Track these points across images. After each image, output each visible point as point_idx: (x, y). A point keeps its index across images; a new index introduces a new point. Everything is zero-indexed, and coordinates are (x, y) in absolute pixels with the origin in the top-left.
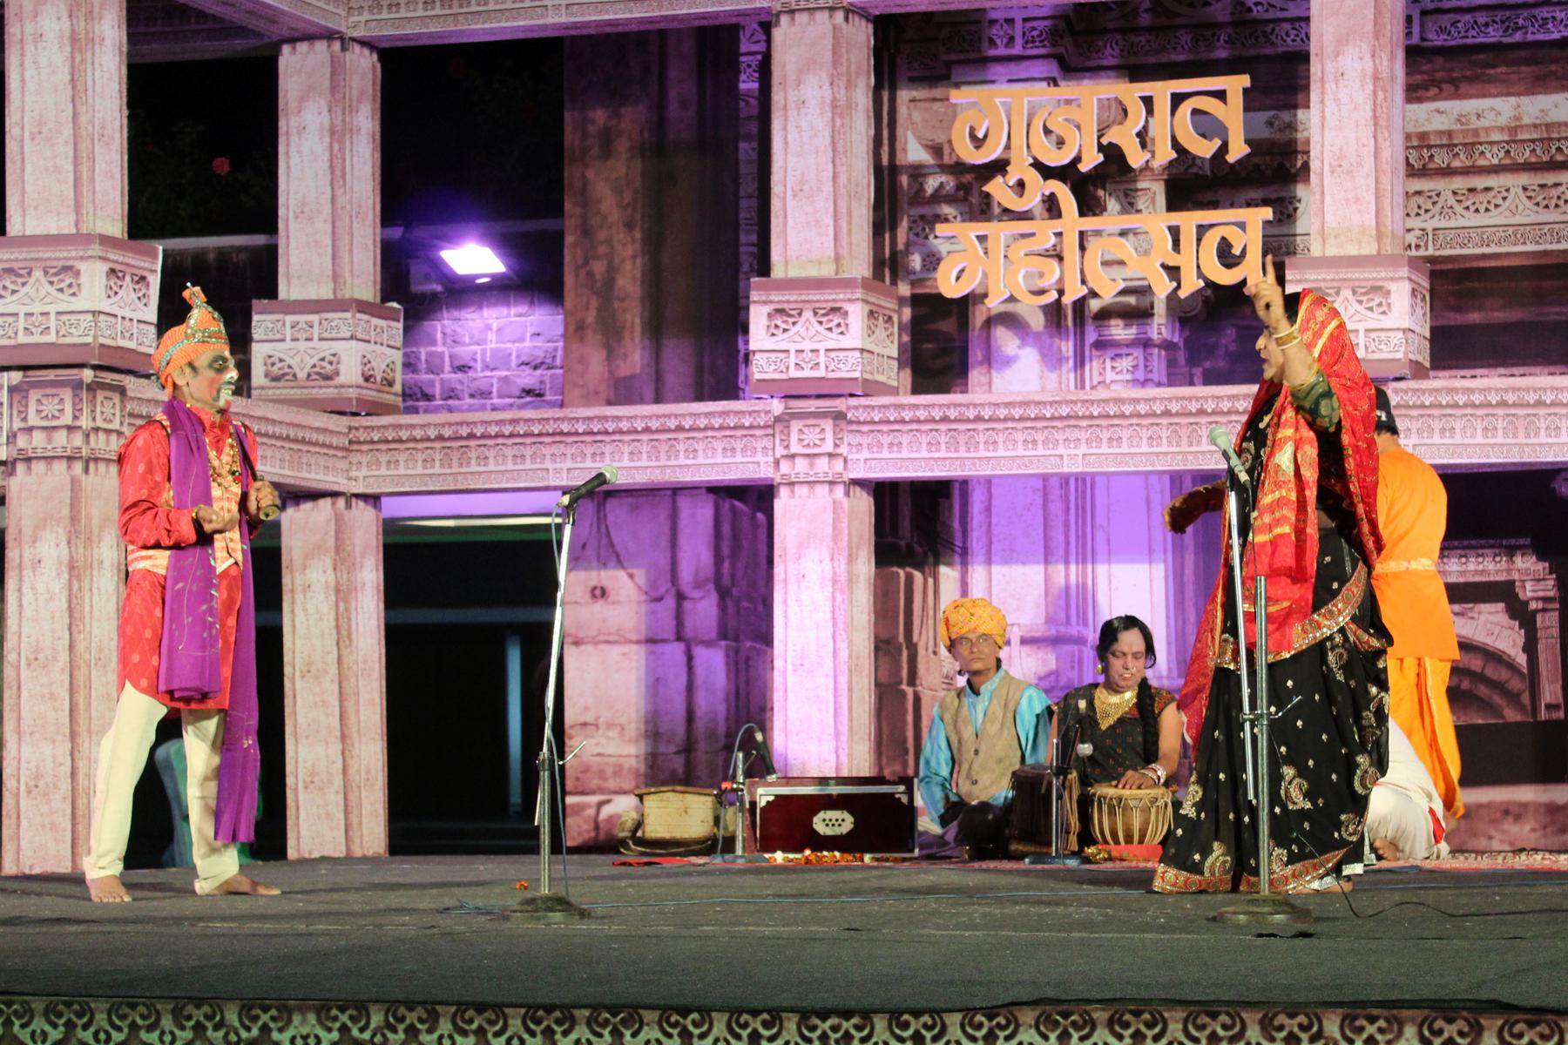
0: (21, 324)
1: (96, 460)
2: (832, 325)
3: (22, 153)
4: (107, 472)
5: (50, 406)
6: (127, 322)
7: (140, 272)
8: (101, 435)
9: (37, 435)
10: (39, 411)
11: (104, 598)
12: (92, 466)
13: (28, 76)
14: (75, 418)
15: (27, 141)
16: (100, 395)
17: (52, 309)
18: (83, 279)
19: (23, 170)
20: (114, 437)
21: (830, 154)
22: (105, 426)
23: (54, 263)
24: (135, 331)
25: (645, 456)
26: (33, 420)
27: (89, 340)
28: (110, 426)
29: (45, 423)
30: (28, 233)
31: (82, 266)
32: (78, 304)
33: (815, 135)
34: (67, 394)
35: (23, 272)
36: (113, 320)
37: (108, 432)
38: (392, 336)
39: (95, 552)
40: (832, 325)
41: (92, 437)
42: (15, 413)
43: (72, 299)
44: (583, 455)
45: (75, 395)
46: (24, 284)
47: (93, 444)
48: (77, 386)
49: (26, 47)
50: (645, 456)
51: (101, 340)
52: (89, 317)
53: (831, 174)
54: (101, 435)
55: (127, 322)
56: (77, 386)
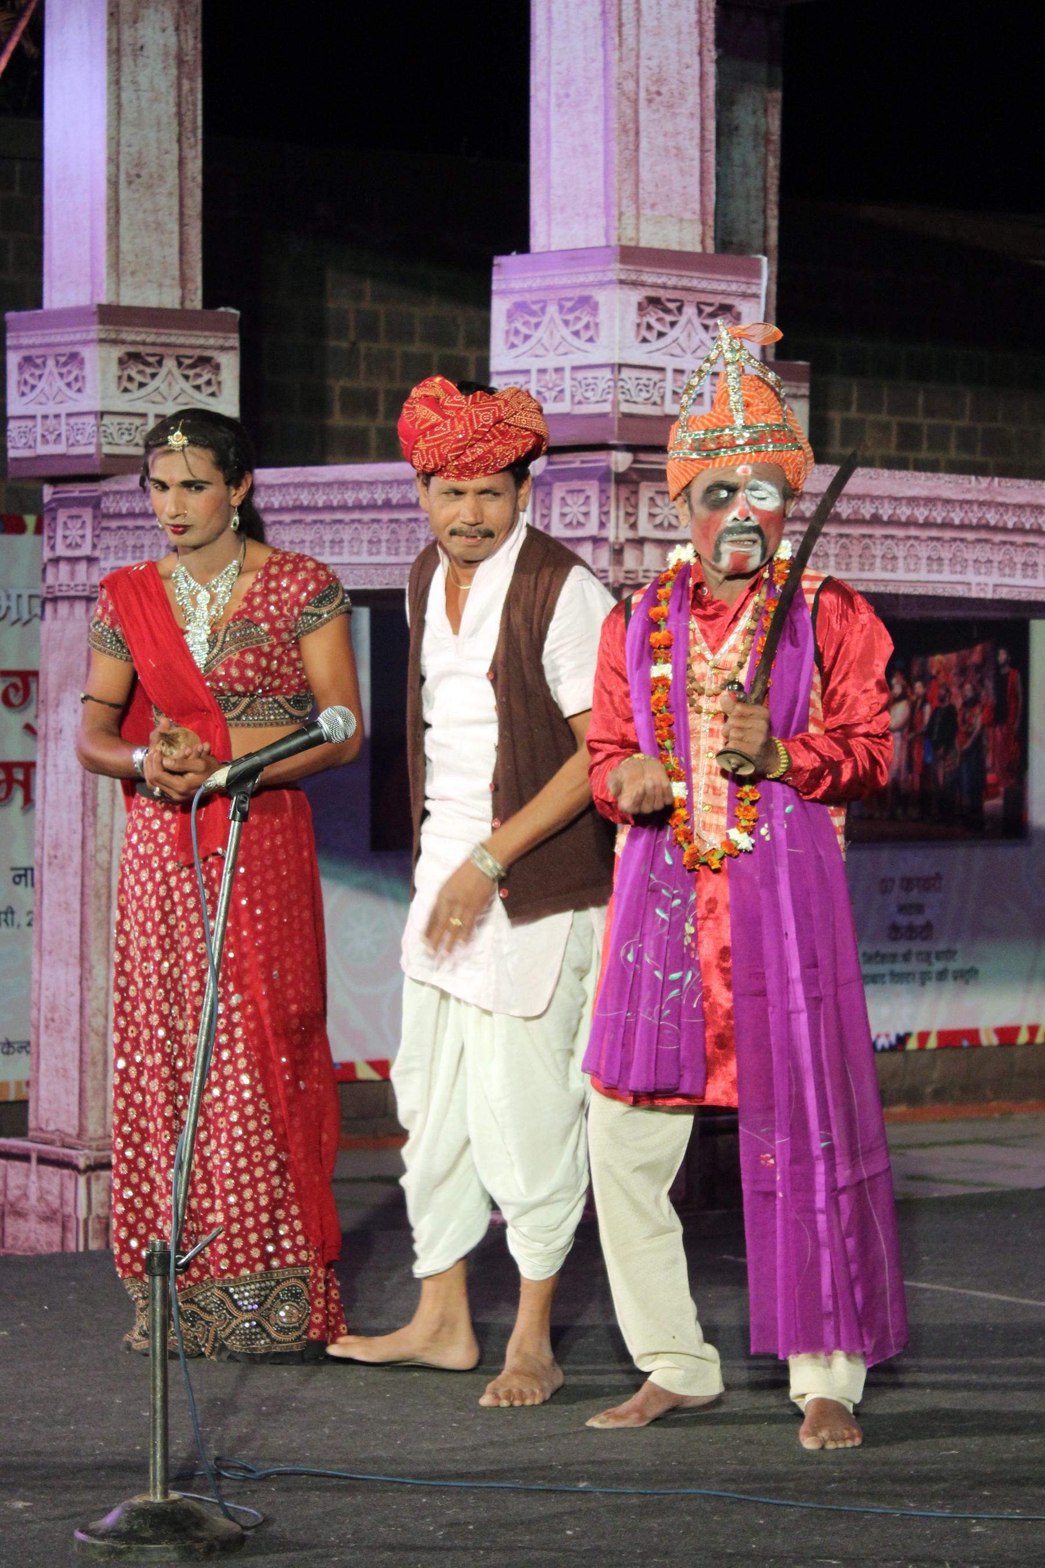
0: (669, 386)
1: (55, 600)
2: (200, 381)
3: (636, 121)
4: (71, 612)
5: (575, 509)
6: (51, 422)
7: (68, 350)
8: (64, 568)
9: (650, 550)
10: (652, 516)
11: (62, 777)
12: (49, 608)
13: (125, 96)
14: (602, 525)
15: (642, 103)
16: (559, 491)
17: (567, 362)
18: (602, 316)
19: (637, 148)
20: (82, 567)
21: (175, 128)
22: (69, 553)
23: (189, 352)
24: (63, 429)
25: (832, 561)
26: (645, 529)
27: (607, 408)
28: (77, 553)
29: (660, 535)
30: (643, 244)
31: (601, 296)
32: (597, 354)
33: (156, 100)
34: (592, 489)
35: (672, 306)
36: (30, 423)
37: (73, 560)
38: (23, 434)
39: (52, 717)
40: (200, 381)
41: (50, 570)
42: (622, 514)
43: (589, 346)
44: (1012, 564)
45: (602, 491)
46: (153, 376)
47: (50, 580)
48: (604, 476)
49: (124, 60)
50: (832, 561)
51: (625, 408)
52: (607, 373)
53: (697, 74)
54: (650, 550)
55: (51, 422)
56: (604, 476)
